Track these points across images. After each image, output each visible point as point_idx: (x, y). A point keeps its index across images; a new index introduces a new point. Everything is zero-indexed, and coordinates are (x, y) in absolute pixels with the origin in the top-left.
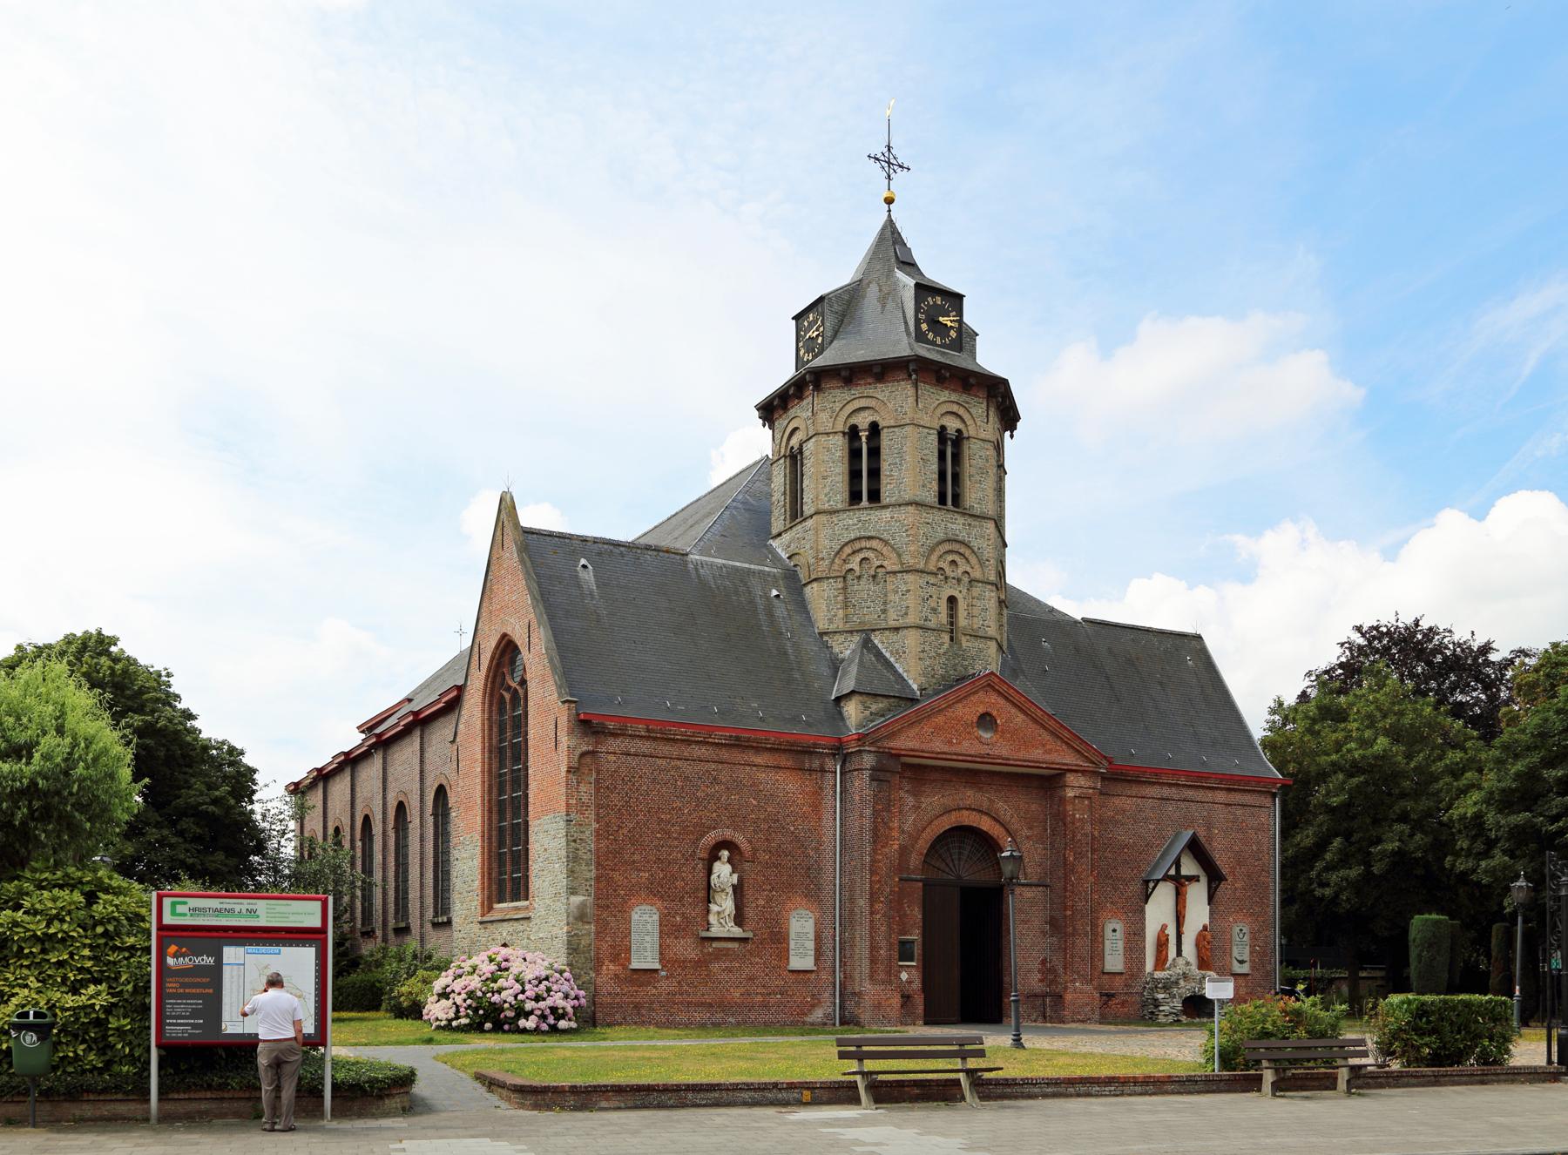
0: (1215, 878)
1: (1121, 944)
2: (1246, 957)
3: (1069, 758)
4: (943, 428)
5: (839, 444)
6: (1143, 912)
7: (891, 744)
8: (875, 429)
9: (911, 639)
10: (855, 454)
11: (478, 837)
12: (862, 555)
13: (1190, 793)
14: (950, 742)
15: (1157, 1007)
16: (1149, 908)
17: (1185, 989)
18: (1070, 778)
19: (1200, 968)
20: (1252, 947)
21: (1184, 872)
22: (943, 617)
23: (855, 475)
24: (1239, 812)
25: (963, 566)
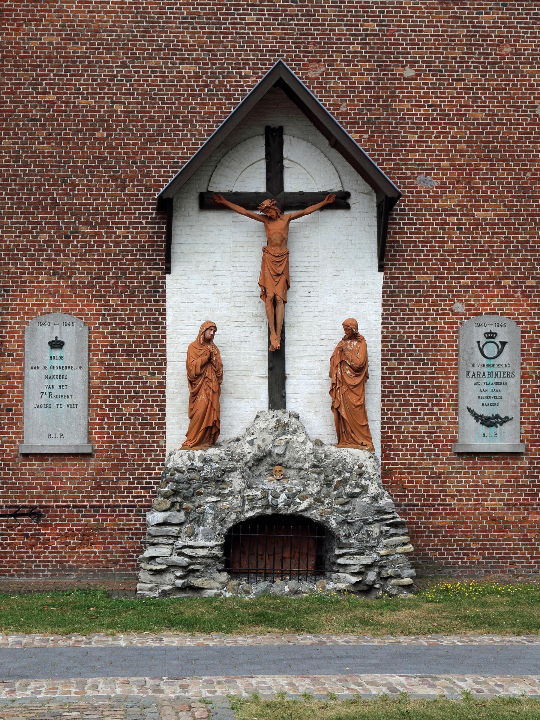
1: (77, 382)
2: (509, 402)
6: (158, 294)
21: (294, 183)
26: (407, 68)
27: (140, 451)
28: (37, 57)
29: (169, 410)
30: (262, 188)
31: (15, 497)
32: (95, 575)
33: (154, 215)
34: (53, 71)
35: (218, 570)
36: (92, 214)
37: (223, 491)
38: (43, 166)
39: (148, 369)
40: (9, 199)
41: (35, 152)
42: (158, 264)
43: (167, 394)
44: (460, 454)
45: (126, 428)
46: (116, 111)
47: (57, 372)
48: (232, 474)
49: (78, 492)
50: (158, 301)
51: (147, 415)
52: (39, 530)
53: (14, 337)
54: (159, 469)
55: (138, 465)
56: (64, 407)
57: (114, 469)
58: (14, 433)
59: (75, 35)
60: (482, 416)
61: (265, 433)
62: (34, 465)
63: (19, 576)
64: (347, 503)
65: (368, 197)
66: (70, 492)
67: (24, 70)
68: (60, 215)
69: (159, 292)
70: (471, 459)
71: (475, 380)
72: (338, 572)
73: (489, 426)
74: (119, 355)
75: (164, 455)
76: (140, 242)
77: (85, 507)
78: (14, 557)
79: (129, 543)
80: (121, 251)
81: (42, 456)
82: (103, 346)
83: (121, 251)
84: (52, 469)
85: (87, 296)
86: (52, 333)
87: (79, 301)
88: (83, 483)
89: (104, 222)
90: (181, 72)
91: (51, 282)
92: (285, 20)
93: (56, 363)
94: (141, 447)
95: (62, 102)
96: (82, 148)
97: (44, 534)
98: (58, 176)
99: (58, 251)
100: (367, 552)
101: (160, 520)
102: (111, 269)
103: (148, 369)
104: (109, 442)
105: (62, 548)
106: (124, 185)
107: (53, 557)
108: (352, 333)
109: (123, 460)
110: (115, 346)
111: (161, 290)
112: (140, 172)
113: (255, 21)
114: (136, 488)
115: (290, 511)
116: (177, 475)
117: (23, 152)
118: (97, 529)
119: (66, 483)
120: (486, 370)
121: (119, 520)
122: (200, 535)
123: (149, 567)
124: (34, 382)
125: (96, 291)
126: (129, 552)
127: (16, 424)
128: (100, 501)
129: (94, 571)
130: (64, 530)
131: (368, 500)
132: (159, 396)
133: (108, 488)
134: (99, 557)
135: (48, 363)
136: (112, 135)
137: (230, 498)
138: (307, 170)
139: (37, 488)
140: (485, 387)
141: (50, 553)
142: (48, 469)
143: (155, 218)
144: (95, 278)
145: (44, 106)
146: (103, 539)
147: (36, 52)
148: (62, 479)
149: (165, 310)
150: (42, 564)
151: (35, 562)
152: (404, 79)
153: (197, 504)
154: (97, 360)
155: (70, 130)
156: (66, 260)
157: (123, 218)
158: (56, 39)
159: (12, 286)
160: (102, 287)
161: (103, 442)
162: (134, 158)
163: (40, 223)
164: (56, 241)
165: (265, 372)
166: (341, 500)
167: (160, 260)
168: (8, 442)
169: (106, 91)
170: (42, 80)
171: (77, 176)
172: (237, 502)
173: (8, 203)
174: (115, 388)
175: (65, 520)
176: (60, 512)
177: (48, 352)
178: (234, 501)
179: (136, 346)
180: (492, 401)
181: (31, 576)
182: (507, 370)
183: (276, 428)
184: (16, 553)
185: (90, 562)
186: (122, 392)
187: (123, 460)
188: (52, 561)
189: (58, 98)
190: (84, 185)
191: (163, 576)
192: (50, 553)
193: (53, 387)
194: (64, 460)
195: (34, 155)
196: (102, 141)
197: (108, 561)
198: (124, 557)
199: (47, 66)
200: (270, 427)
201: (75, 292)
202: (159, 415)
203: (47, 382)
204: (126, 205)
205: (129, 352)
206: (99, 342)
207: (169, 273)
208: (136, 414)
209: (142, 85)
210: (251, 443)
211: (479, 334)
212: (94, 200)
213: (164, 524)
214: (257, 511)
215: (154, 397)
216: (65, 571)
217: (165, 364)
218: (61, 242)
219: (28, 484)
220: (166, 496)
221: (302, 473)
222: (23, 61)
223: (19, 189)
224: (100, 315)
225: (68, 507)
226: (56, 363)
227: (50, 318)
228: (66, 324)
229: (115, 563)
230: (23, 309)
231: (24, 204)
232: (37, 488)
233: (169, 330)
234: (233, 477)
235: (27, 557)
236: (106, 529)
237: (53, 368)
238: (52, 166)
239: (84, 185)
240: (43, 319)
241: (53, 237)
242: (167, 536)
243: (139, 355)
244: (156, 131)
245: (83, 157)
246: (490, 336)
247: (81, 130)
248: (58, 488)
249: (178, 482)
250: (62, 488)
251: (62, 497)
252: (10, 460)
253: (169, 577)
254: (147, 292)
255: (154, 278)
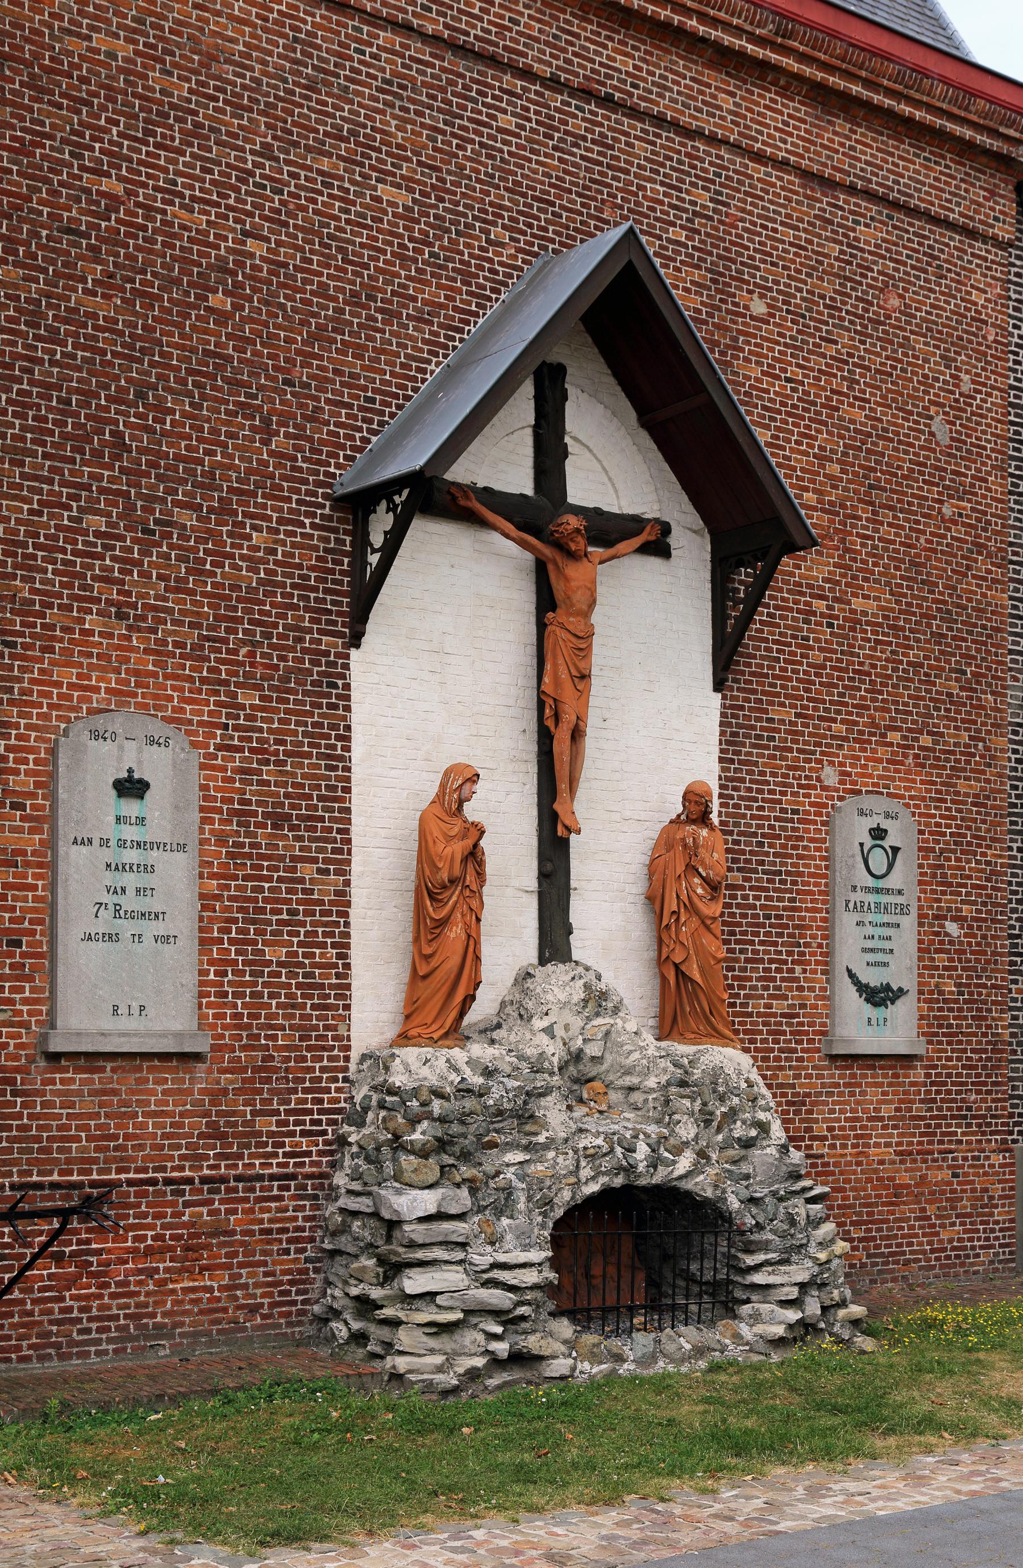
0: (748, 529)
1: (176, 882)
2: (901, 971)
6: (333, 691)
15: (392, 1269)
16: (376, 673)
17: (573, 1153)
19: (669, 1026)
20: (930, 920)
21: (587, 486)
24: (867, 235)
26: (755, 296)
27: (298, 1048)
28: (83, 80)
29: (357, 956)
31: (29, 1162)
32: (211, 1343)
33: (327, 511)
34: (117, 123)
35: (550, 1314)
36: (202, 485)
37: (534, 1139)
38: (94, 350)
39: (315, 860)
40: (15, 415)
41: (76, 311)
42: (334, 623)
43: (353, 919)
44: (833, 1058)
45: (271, 996)
46: (252, 256)
47: (131, 856)
48: (543, 1102)
49: (171, 1147)
50: (335, 707)
51: (314, 965)
52: (88, 1242)
53: (26, 762)
54: (338, 1090)
55: (296, 1080)
56: (148, 940)
57: (247, 1090)
58: (25, 1001)
59: (165, 51)
60: (867, 986)
61: (567, 1011)
62: (72, 1080)
63: (41, 1358)
64: (743, 1158)
65: (698, 539)
66: (153, 1147)
67: (50, 103)
68: (134, 474)
69: (335, 686)
70: (847, 1068)
71: (856, 917)
72: (748, 1301)
73: (876, 1005)
74: (258, 825)
75: (347, 1059)
76: (300, 566)
77: (190, 1181)
78: (31, 1313)
79: (282, 1263)
80: (260, 581)
81: (92, 1060)
82: (224, 800)
83: (260, 581)
84: (115, 1092)
85: (191, 679)
86: (120, 759)
87: (174, 688)
88: (182, 1125)
89: (225, 510)
90: (378, 199)
91: (111, 636)
92: (565, 141)
93: (131, 833)
94: (302, 1039)
95: (138, 204)
96: (181, 326)
97: (98, 1252)
98: (128, 380)
99: (127, 563)
100: (794, 1258)
101: (432, 1209)
102: (239, 620)
103: (315, 860)
104: (238, 1027)
105: (140, 1283)
106: (267, 432)
107: (120, 1307)
109: (265, 1069)
110: (249, 802)
111: (340, 682)
112: (301, 406)
113: (513, 128)
114: (292, 1134)
115: (657, 1179)
116: (437, 1106)
117: (49, 305)
118: (213, 1235)
119: (143, 1126)
120: (872, 898)
121: (262, 1210)
122: (509, 1237)
123: (423, 1317)
124: (81, 876)
125: (210, 670)
126: (281, 1283)
127: (30, 979)
128: (217, 1167)
129: (208, 1333)
130: (143, 1239)
131: (772, 1151)
132: (337, 924)
133: (235, 1135)
134: (218, 1299)
135: (112, 831)
136: (242, 308)
137: (551, 1154)
139: (78, 1139)
140: (870, 930)
141: (113, 1296)
142: (104, 1092)
143: (330, 518)
144: (208, 639)
145: (98, 204)
146: (228, 1255)
147: (79, 68)
148: (135, 1115)
149: (348, 728)
150: (94, 1326)
151: (79, 1320)
152: (752, 317)
153: (490, 1169)
154: (212, 832)
155: (154, 274)
156: (145, 585)
157: (264, 506)
158: (124, 50)
159: (22, 635)
160: (223, 662)
161: (225, 1027)
162: (288, 371)
163: (88, 488)
164: (122, 538)
165: (532, 882)
166: (731, 1152)
167: (339, 614)
168: (12, 1024)
169: (231, 202)
170: (93, 138)
171: (167, 389)
172: (565, 1163)
173: (12, 426)
174: (248, 899)
175: (145, 1216)
176: (137, 1195)
177: (112, 805)
178: (560, 1159)
179: (293, 806)
180: (880, 957)
181: (69, 1356)
182: (900, 900)
183: (586, 1001)
184: (34, 1302)
185: (201, 1312)
186: (262, 910)
187: (265, 1069)
188: (117, 1317)
189: (128, 193)
190: (184, 414)
191: (457, 1337)
192: (113, 1296)
193: (123, 890)
194: (140, 1069)
195: (71, 317)
196: (223, 317)
197: (239, 1307)
198: (270, 1295)
199: (103, 108)
200: (576, 999)
201: (163, 665)
202: (335, 966)
203: (110, 878)
204: (272, 476)
205: (279, 820)
206: (217, 789)
207: (358, 646)
208: (290, 964)
209: (304, 209)
210: (549, 1031)
211: (860, 830)
212: (207, 452)
213: (440, 1216)
214: (603, 1180)
215: (326, 924)
216: (146, 1338)
217: (349, 853)
218: (135, 540)
219: (60, 1128)
220: (423, 1154)
221: (637, 1097)
222: (51, 81)
223: (39, 395)
224: (217, 725)
225: (153, 1182)
226: (131, 833)
227: (117, 723)
228: (152, 741)
229: (254, 1309)
230: (48, 695)
231: (52, 433)
232: (78, 1139)
233: (357, 774)
234: (546, 1108)
235: (62, 1311)
236: (233, 1233)
237: (122, 844)
238: (115, 354)
239: (184, 414)
240: (100, 722)
241: (115, 525)
242: (445, 1244)
243: (298, 828)
244: (332, 319)
245: (183, 347)
246: (878, 833)
247: (178, 282)
248: (127, 1137)
249: (442, 1120)
250: (135, 1137)
251: (134, 1160)
252: (17, 1070)
253: (471, 1338)
254: (313, 683)
255: (327, 654)
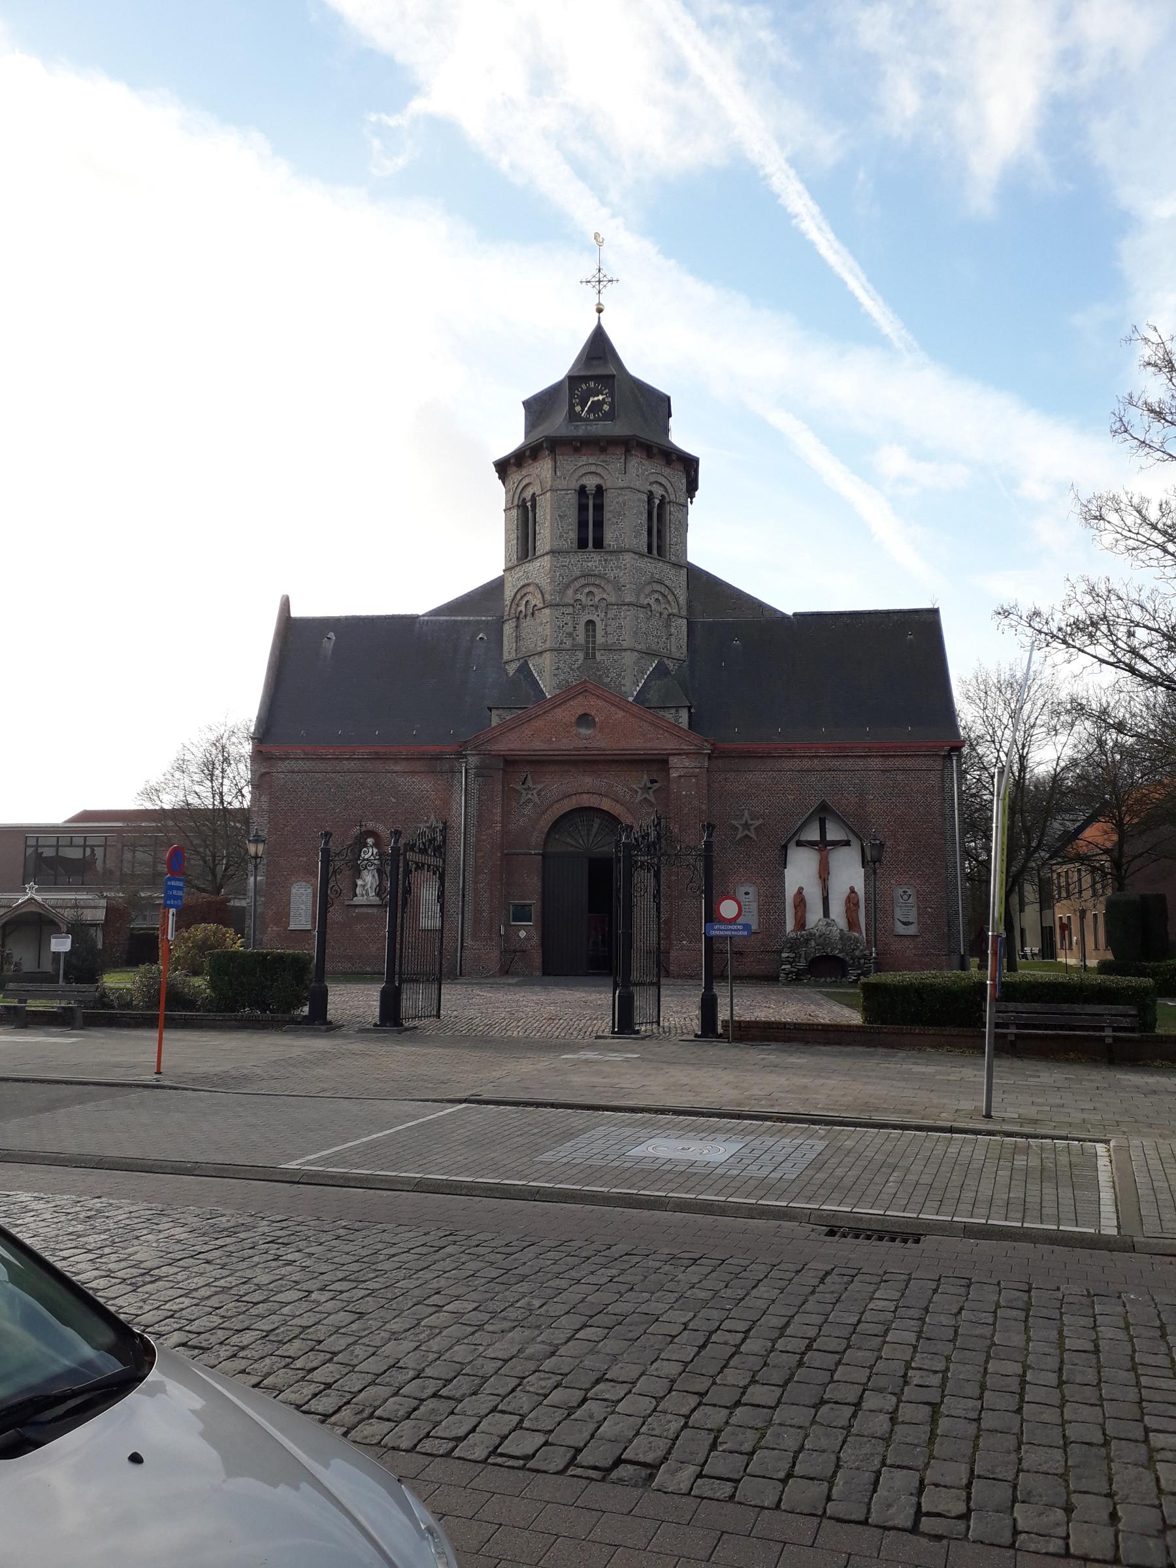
1: (754, 906)
2: (913, 916)
3: (671, 744)
4: (583, 488)
5: (572, 499)
6: (782, 876)
7: (495, 747)
8: (600, 490)
9: (547, 659)
10: (582, 508)
11: (1112, 1074)
12: (587, 590)
13: (836, 763)
14: (550, 741)
18: (673, 761)
21: (830, 837)
22: (581, 639)
23: (582, 525)
24: (900, 777)
25: (599, 595)
30: (818, 839)
108: (852, 890)
138: (834, 833)
211: (900, 891)
